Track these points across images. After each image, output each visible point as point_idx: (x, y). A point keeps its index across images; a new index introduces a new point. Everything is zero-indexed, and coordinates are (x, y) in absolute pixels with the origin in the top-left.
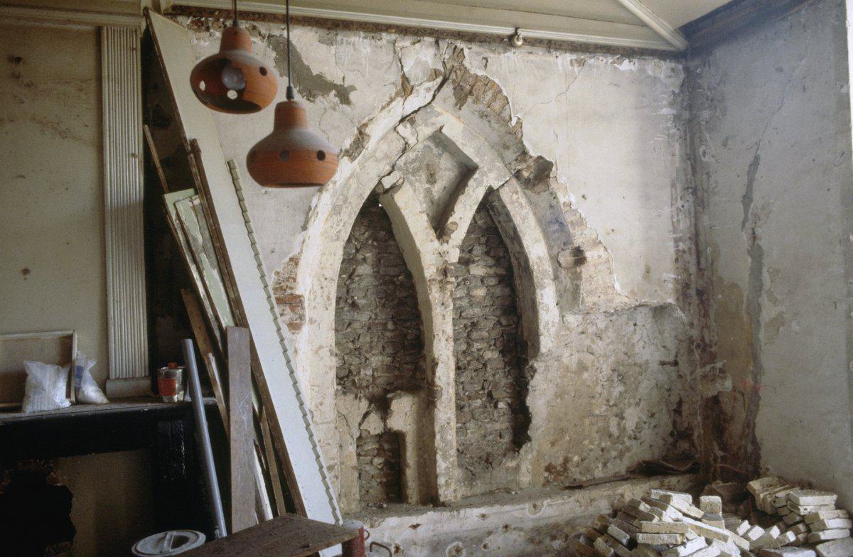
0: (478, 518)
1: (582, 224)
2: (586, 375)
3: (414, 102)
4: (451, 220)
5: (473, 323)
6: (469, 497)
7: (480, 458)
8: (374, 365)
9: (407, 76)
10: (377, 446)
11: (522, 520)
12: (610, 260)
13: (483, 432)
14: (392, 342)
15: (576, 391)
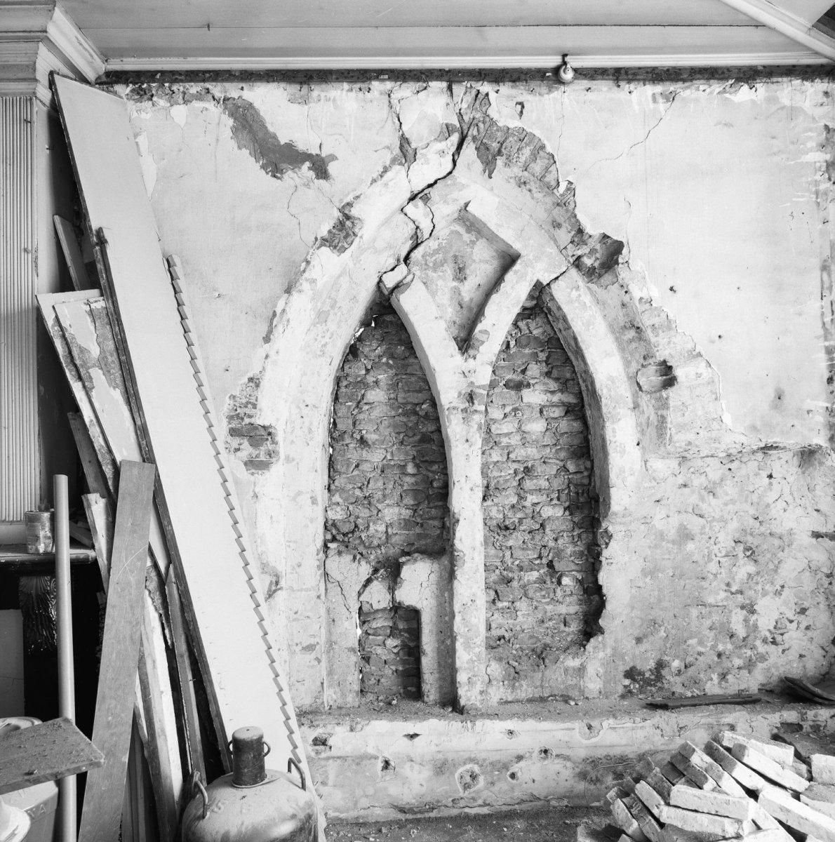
0: (502, 735)
1: (670, 329)
2: (690, 546)
3: (422, 173)
4: (479, 327)
5: (526, 468)
6: (510, 702)
7: (533, 650)
8: (387, 519)
9: (407, 135)
10: (391, 624)
11: (568, 745)
12: (716, 380)
13: (540, 616)
14: (415, 492)
15: (675, 568)
